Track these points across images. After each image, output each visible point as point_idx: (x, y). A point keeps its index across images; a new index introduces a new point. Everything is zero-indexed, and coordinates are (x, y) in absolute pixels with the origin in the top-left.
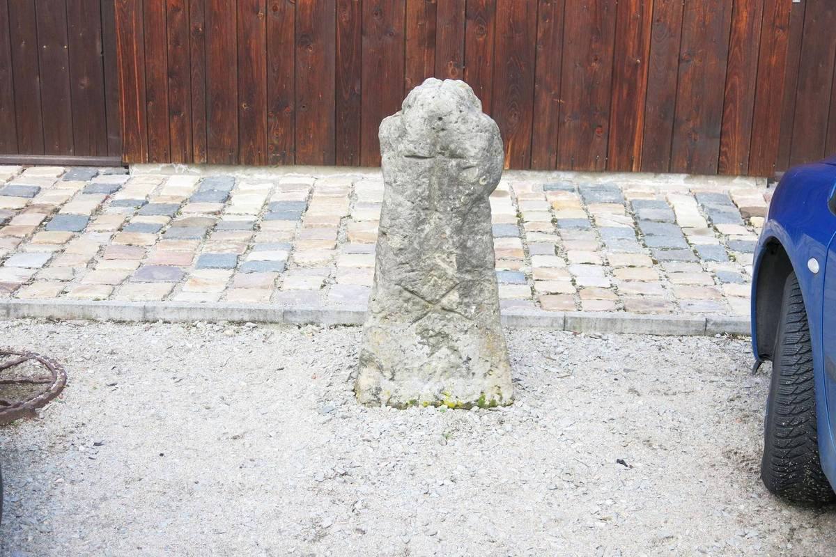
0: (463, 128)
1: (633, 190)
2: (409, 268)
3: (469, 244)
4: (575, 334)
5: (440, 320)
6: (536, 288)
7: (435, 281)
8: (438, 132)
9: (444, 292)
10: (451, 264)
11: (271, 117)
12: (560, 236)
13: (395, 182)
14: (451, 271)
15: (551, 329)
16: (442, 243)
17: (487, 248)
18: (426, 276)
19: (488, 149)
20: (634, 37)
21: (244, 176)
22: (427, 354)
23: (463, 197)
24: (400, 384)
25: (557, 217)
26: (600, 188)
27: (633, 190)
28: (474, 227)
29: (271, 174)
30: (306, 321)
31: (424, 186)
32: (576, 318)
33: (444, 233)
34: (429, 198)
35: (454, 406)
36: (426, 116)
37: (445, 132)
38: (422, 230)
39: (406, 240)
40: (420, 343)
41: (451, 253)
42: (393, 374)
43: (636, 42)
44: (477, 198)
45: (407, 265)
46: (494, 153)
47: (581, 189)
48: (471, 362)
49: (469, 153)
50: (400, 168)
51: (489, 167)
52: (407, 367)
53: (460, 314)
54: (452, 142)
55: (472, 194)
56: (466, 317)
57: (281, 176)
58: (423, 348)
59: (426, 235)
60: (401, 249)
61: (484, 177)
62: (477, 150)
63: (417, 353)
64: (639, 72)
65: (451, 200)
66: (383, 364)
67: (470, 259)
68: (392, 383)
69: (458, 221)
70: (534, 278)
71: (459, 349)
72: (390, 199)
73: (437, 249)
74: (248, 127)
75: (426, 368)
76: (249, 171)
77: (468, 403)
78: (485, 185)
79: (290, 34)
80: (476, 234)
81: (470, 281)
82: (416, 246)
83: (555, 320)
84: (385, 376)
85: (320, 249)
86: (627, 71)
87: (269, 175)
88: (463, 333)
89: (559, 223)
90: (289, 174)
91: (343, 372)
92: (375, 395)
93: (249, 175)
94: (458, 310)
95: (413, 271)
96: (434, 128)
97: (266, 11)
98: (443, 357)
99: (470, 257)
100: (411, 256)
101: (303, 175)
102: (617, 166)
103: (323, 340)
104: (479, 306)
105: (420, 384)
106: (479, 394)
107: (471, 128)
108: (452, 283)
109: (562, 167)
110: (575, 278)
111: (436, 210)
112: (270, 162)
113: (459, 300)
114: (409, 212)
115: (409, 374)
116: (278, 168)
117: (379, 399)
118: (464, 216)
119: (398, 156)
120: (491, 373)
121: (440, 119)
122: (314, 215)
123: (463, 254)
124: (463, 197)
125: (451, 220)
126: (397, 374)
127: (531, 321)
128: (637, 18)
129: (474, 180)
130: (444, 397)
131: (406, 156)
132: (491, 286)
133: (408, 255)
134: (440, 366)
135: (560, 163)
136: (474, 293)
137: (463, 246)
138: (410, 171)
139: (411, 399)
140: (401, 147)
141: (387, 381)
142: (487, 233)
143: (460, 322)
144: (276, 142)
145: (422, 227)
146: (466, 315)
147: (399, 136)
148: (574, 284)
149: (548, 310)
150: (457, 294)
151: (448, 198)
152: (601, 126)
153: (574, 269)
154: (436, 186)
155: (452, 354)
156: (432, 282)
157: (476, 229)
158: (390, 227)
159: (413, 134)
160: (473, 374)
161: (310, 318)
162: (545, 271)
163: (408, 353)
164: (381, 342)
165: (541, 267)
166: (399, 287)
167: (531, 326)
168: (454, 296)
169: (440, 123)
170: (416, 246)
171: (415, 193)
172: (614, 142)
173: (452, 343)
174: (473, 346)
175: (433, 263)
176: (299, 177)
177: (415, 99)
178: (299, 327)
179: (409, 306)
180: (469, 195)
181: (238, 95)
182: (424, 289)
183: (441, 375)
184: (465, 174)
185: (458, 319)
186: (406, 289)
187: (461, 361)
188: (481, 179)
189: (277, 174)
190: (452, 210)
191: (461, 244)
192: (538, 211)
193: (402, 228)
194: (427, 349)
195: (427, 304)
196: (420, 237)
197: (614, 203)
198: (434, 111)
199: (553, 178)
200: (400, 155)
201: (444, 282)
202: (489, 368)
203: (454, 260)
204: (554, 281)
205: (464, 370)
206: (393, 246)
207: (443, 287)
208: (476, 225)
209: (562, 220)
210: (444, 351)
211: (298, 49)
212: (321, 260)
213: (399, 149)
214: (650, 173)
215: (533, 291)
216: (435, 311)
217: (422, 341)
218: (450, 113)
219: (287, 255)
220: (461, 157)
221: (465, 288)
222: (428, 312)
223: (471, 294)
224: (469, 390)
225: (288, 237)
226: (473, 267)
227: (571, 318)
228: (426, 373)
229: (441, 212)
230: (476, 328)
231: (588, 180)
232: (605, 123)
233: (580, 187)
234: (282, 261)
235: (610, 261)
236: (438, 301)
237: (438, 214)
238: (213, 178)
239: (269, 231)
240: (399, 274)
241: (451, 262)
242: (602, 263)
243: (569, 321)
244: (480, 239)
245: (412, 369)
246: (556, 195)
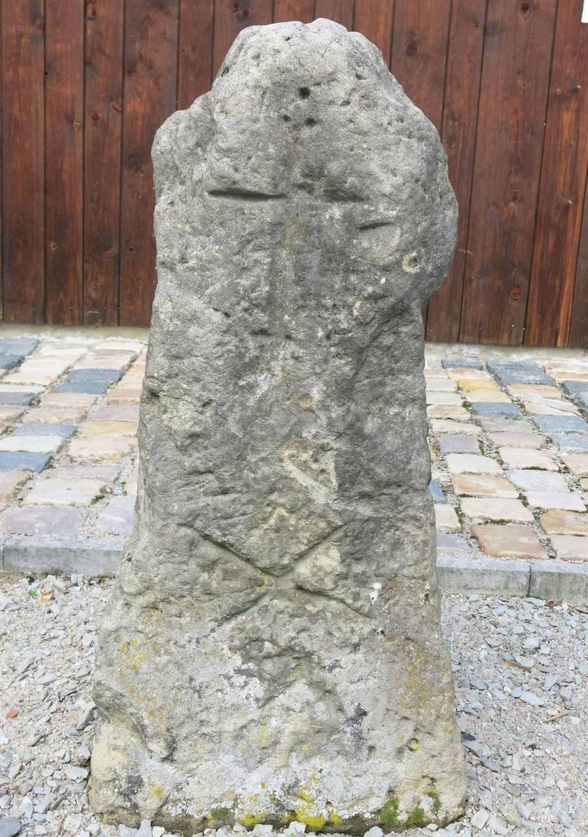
0: (364, 119)
1: (560, 370)
2: (215, 485)
3: (370, 425)
4: (550, 605)
5: (292, 616)
6: (464, 509)
7: (282, 518)
8: (296, 127)
9: (303, 548)
10: (321, 477)
11: (87, 261)
12: (479, 425)
13: (183, 260)
14: (322, 496)
15: (506, 593)
16: (300, 423)
17: (412, 438)
18: (258, 507)
19: (424, 182)
20: (566, 169)
21: (53, 339)
22: (257, 700)
23: (358, 304)
24: (189, 771)
25: (469, 400)
26: (516, 366)
27: (560, 370)
28: (382, 384)
29: (88, 337)
30: (46, 567)
31: (257, 271)
32: (552, 574)
33: (307, 396)
34: (269, 303)
35: (320, 825)
36: (266, 82)
37: (316, 128)
38: (251, 388)
39: (209, 412)
40: (239, 672)
41: (324, 448)
42: (172, 747)
43: (568, 177)
44: (393, 308)
45: (211, 477)
46: (438, 200)
47: (492, 366)
48: (366, 721)
49: (376, 187)
50: (197, 224)
51: (426, 231)
52: (205, 730)
53: (342, 601)
54: (335, 154)
55: (383, 297)
56: (357, 610)
57: (101, 340)
58: (246, 684)
59: (260, 401)
60: (194, 436)
61: (414, 254)
62: (399, 180)
63: (233, 696)
64: (571, 214)
65: (327, 309)
66: (146, 722)
67: (372, 465)
68: (169, 768)
69: (344, 366)
70: (458, 492)
71: (338, 689)
72: (169, 305)
73: (288, 436)
74: (57, 273)
75: (253, 734)
76: (59, 332)
77: (357, 817)
78: (417, 275)
79: (116, 152)
80: (388, 403)
81: (368, 520)
82: (234, 428)
83: (512, 576)
84: (150, 751)
85: (116, 435)
86: (555, 215)
87: (85, 339)
88: (348, 650)
89: (475, 408)
90: (110, 339)
91: (80, 702)
92: (126, 795)
93: (59, 338)
94: (337, 593)
95: (225, 492)
96: (286, 118)
97: (84, 120)
98: (298, 707)
99: (372, 459)
100: (219, 453)
101: (129, 340)
102: (537, 340)
103: (68, 610)
104: (391, 582)
105: (239, 771)
106: (383, 794)
107: (385, 120)
108: (323, 525)
109: (466, 338)
110: (524, 494)
111: (288, 337)
112: (86, 321)
113: (340, 569)
114: (216, 337)
115: (208, 746)
116: (98, 329)
117: (135, 806)
118: (359, 354)
119: (194, 196)
120: (414, 745)
121: (304, 93)
122: (126, 387)
123: (353, 453)
124: (358, 304)
125: (326, 361)
126: (183, 746)
127: (468, 578)
128: (571, 145)
129: (389, 259)
130: (297, 804)
131: (214, 193)
132: (418, 532)
133: (212, 450)
134: (290, 728)
135: (464, 332)
136: (379, 550)
137: (353, 432)
138: (221, 232)
139: (214, 806)
140: (201, 170)
141: (155, 763)
142: (414, 400)
143: (341, 625)
144: (94, 295)
145: (250, 379)
146: (358, 604)
147: (198, 145)
148: (526, 504)
149: (496, 556)
150: (335, 553)
151: (320, 306)
152: (518, 287)
153: (520, 478)
154: (290, 274)
155: (320, 699)
156: (272, 521)
157: (388, 389)
158: (169, 377)
159: (230, 136)
160: (371, 748)
161: (53, 563)
162: (473, 480)
163: (210, 697)
164: (144, 667)
165: (464, 473)
166: (189, 531)
167: (466, 587)
168: (329, 559)
169: (303, 103)
170: (234, 428)
171: (233, 288)
172: (534, 307)
173: (318, 674)
174: (372, 682)
175: (275, 474)
176: (124, 342)
177: (242, 45)
178: (32, 580)
179: (214, 580)
180: (374, 298)
181: (45, 232)
182: (253, 539)
183: (291, 751)
184: (364, 241)
185: (336, 616)
186: (207, 537)
187: (342, 718)
188: (407, 258)
189: (96, 338)
190: (328, 337)
191: (350, 426)
192: (440, 391)
193: (197, 380)
194: (257, 688)
195: (258, 574)
196: (244, 406)
197: (540, 384)
198: (289, 71)
199: (454, 353)
200: (198, 192)
201: (303, 523)
202: (409, 734)
203: (331, 467)
204: (489, 497)
205: (347, 739)
206: (175, 427)
207: (301, 535)
208: (388, 380)
209: (478, 404)
210: (300, 690)
211: (125, 172)
212: (112, 453)
213: (196, 177)
214: (577, 350)
215: (461, 515)
216: (280, 594)
217: (244, 667)
218: (331, 78)
219: (59, 444)
220: (355, 197)
221: (356, 538)
222: (264, 595)
223: (370, 553)
224: (360, 786)
225: (74, 415)
226: (378, 484)
227: (543, 574)
228: (254, 745)
229: (300, 343)
230: (380, 637)
231: (498, 357)
232: (523, 281)
233: (489, 364)
234: (48, 454)
235: (569, 465)
236: (287, 569)
237: (292, 347)
238: (10, 340)
239: (52, 407)
240: (190, 499)
241: (323, 471)
242: (557, 469)
243: (539, 580)
244: (397, 414)
245: (220, 734)
246: (461, 372)
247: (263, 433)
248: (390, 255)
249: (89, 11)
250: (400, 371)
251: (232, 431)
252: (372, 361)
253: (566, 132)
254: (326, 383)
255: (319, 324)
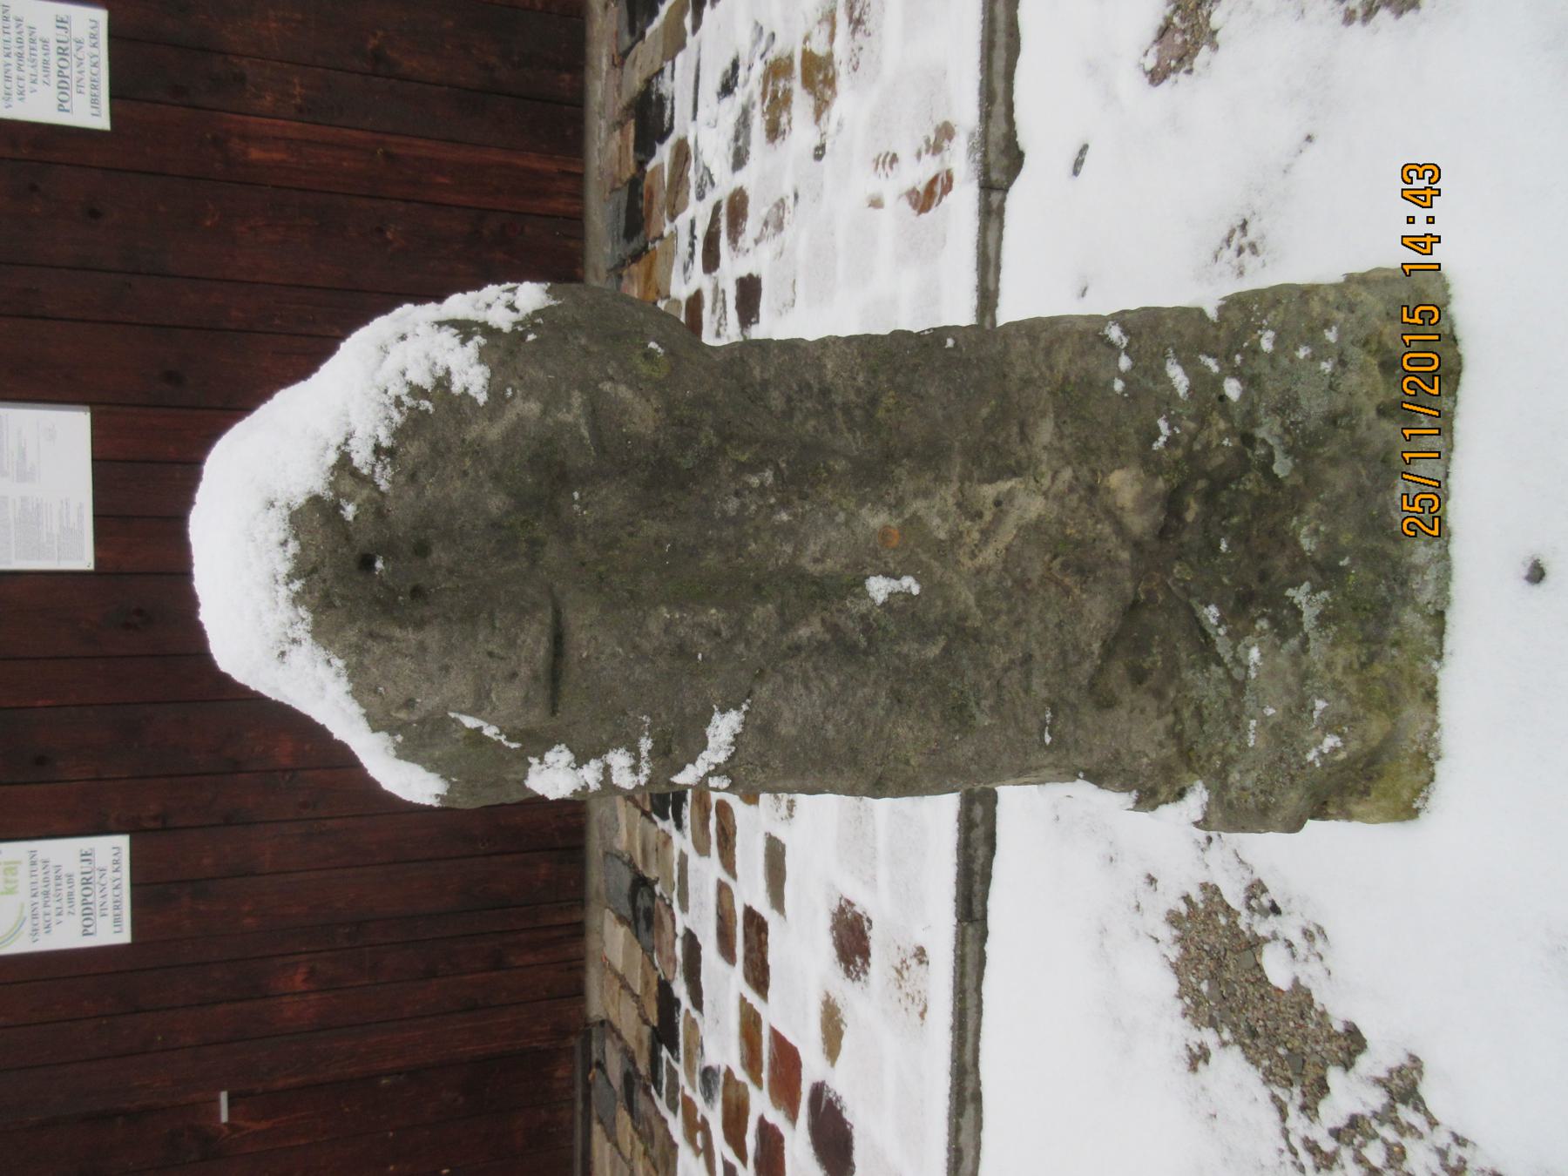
33: (884, 533)
170: (933, 651)
247: (939, 603)
248: (648, 400)
249: (152, 825)
250: (821, 380)
251: (937, 652)
252: (814, 427)
253: (277, 156)
254: (861, 502)
255: (768, 518)
